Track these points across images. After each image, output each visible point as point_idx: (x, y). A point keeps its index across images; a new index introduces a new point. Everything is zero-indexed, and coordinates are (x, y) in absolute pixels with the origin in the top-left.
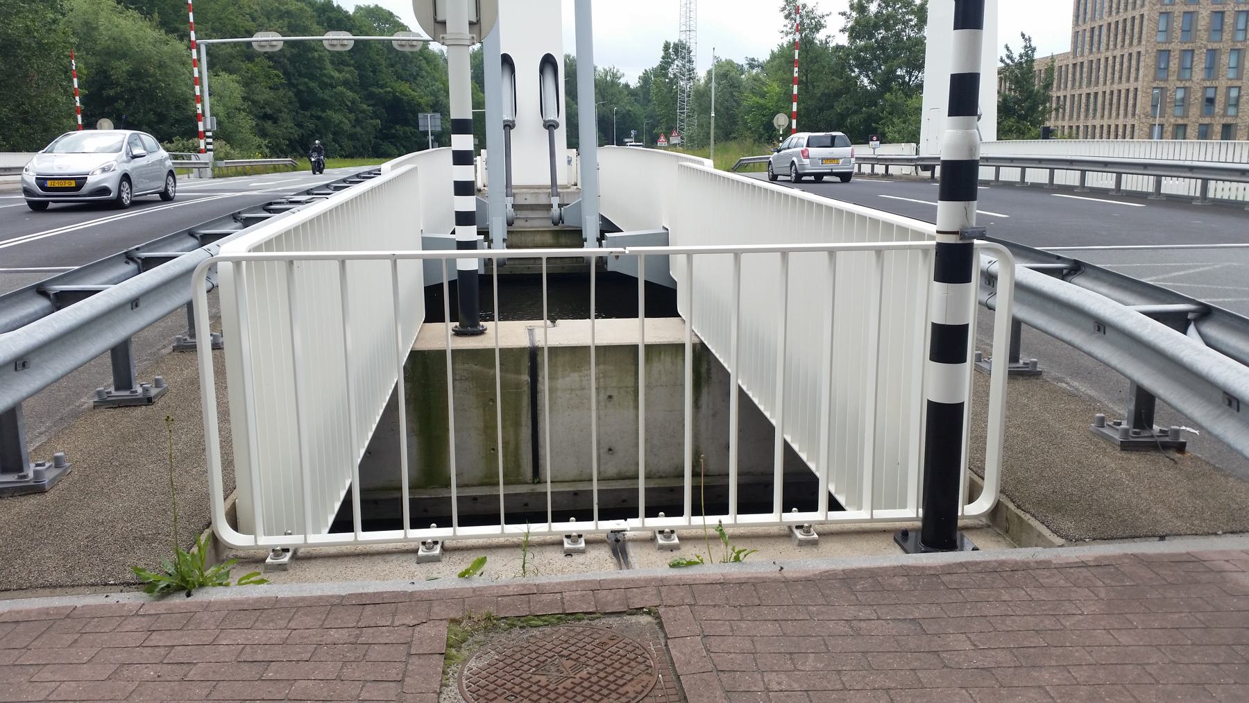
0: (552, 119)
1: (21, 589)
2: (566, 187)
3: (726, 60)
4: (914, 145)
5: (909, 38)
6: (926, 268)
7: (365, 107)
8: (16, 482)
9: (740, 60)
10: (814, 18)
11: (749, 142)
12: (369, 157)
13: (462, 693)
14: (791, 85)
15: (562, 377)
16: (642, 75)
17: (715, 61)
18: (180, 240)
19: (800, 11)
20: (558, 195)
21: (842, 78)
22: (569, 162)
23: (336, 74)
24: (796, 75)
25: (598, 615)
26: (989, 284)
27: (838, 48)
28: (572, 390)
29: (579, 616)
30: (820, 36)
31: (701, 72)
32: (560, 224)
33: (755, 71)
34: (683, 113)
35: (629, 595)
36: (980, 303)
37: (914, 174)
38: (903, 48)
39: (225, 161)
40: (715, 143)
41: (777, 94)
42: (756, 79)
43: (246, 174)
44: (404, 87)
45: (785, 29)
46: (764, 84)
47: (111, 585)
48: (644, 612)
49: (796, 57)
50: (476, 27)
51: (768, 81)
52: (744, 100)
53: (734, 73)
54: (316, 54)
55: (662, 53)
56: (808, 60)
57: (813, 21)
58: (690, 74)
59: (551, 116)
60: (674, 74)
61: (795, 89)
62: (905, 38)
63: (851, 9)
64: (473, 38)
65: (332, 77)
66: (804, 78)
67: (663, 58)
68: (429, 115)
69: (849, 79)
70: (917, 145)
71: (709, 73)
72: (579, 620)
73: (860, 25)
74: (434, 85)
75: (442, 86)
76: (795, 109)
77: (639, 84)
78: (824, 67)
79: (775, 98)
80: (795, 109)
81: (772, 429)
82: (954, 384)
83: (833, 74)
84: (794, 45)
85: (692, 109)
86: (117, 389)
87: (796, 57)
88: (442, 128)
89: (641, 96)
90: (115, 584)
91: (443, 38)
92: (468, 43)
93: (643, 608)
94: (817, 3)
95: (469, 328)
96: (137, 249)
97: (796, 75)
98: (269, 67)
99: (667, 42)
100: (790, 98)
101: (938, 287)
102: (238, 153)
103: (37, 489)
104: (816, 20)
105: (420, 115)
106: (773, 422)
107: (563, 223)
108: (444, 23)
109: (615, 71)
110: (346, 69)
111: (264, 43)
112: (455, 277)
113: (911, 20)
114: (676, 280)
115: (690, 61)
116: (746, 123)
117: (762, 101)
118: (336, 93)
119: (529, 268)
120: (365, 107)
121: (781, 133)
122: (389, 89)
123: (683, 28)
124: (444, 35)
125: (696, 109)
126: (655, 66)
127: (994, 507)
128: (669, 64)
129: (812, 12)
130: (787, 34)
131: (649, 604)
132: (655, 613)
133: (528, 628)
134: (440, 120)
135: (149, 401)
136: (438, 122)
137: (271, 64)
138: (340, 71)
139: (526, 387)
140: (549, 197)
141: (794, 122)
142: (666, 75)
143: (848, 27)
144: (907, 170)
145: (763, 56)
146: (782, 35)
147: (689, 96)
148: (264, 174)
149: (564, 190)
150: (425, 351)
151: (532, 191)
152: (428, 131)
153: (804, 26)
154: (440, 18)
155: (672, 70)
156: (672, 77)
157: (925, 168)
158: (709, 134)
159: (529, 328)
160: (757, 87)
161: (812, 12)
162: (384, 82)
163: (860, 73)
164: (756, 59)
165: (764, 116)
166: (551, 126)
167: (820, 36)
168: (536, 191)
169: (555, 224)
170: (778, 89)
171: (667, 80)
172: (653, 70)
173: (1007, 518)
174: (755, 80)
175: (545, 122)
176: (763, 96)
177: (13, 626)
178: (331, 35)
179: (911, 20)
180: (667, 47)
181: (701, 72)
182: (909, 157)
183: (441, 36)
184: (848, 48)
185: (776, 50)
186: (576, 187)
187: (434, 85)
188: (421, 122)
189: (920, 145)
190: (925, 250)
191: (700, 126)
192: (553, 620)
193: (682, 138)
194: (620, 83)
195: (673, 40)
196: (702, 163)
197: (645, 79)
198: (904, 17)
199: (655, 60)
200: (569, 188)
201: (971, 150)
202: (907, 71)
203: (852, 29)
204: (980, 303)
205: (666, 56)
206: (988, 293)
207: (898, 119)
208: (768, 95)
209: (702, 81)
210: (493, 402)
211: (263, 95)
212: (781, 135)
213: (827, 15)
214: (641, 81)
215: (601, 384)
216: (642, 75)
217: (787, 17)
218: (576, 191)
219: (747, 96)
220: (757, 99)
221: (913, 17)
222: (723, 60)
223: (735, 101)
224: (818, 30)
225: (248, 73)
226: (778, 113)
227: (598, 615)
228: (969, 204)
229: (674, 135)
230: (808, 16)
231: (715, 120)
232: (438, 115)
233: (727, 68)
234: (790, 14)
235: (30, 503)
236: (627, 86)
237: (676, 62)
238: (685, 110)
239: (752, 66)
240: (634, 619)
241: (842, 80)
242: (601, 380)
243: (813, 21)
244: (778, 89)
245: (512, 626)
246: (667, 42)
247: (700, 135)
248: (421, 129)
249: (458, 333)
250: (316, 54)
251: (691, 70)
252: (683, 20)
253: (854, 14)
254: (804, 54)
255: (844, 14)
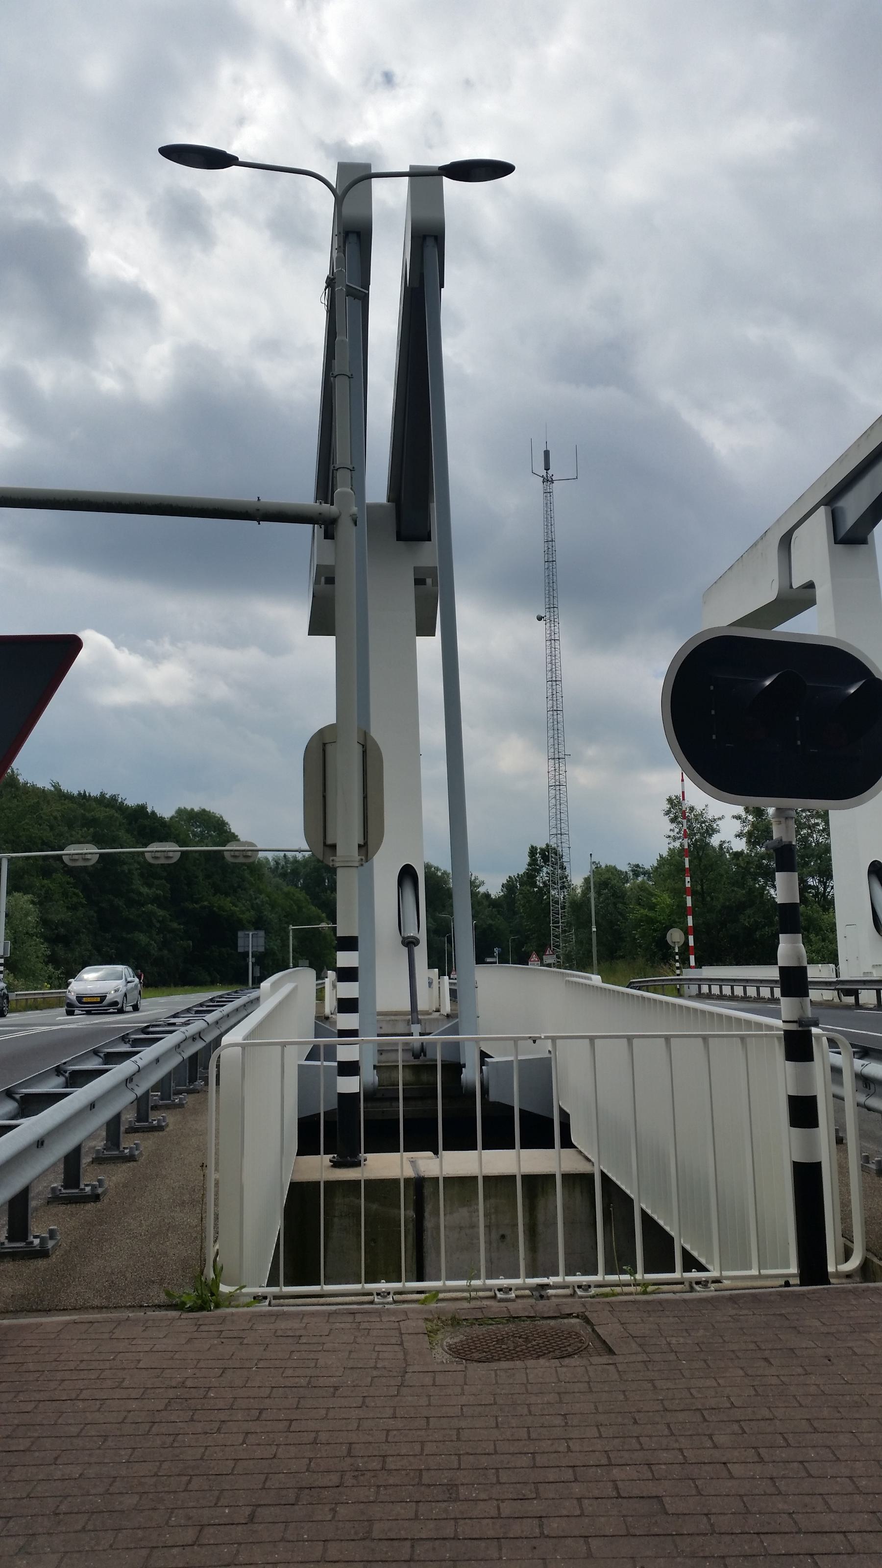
0: (412, 934)
1: (75, 1309)
2: (427, 1013)
3: (606, 866)
4: (832, 966)
5: (818, 843)
6: (779, 1051)
7: (175, 925)
8: (25, 1247)
9: (623, 867)
10: (704, 822)
11: (640, 961)
12: (176, 985)
13: (444, 1350)
14: (684, 896)
15: (450, 1213)
16: (505, 882)
17: (594, 867)
18: (88, 1058)
19: (687, 814)
20: (419, 1022)
21: (744, 889)
22: (430, 984)
23: (145, 890)
24: (688, 885)
25: (537, 1318)
26: (866, 1087)
27: (738, 855)
28: (461, 1228)
29: (523, 1318)
30: (715, 841)
31: (577, 880)
32: (422, 1058)
33: (640, 879)
34: (558, 927)
35: (560, 1308)
36: (858, 1105)
37: (837, 1000)
38: (812, 855)
39: (16, 993)
40: (599, 963)
41: (668, 906)
42: (642, 887)
43: (37, 1008)
44: (226, 903)
45: (672, 834)
46: (652, 895)
47: (146, 1306)
48: (573, 1317)
49: (687, 866)
50: (363, 850)
51: (657, 892)
52: (630, 913)
53: (615, 881)
54: (126, 868)
55: (528, 860)
56: (703, 868)
57: (703, 825)
58: (565, 885)
59: (411, 932)
60: (544, 883)
61: (689, 901)
62: (814, 844)
63: (747, 812)
64: (362, 860)
65: (140, 894)
66: (699, 888)
67: (529, 865)
68: (251, 934)
69: (751, 890)
70: (836, 966)
71: (587, 880)
72: (524, 1321)
73: (758, 830)
74: (259, 898)
75: (267, 899)
76: (690, 923)
77: (502, 894)
78: (722, 876)
79: (667, 911)
80: (690, 923)
81: (671, 1239)
82: (811, 1145)
83: (733, 885)
84: (682, 852)
85: (568, 922)
86: (65, 1187)
87: (687, 866)
88: (265, 949)
89: (505, 906)
90: (148, 1306)
91: (333, 860)
92: (357, 864)
93: (572, 1314)
94: (706, 806)
95: (348, 1159)
96: (65, 1063)
97: (688, 885)
98: (68, 883)
99: (532, 847)
100: (683, 911)
101: (789, 1064)
102: (22, 985)
103: (43, 1253)
104: (707, 824)
105: (240, 934)
106: (672, 1234)
107: (425, 1055)
108: (333, 847)
109: (473, 878)
110: (157, 882)
111: (76, 857)
112: (334, 1104)
113: (818, 824)
114: (568, 1111)
115: (563, 868)
116: (635, 939)
117: (651, 914)
118: (144, 912)
119: (383, 1112)
120: (175, 925)
121: (677, 951)
122: (206, 903)
123: (554, 831)
124: (334, 858)
125: (573, 922)
126: (521, 873)
127: (862, 1263)
128: (539, 871)
129: (702, 814)
130: (675, 839)
131: (576, 1312)
132: (582, 1316)
133: (486, 1326)
134: (263, 939)
135: (96, 1198)
136: (262, 941)
137: (72, 880)
138: (150, 886)
139: (411, 1224)
140: (408, 1025)
141: (691, 938)
142: (534, 885)
143: (744, 831)
144: (828, 995)
145: (649, 862)
146: (668, 840)
147: (563, 908)
148: (57, 1007)
149: (426, 1017)
150: (303, 1182)
151: (388, 1018)
152: (248, 953)
153: (693, 831)
154: (329, 841)
155: (543, 876)
156: (541, 885)
157: (848, 993)
158: (591, 951)
159: (412, 1160)
160: (643, 897)
161: (702, 814)
162: (201, 896)
163: (766, 883)
164: (641, 866)
165: (655, 930)
166: (410, 943)
167: (715, 841)
168: (393, 1018)
169: (416, 1056)
170: (669, 901)
171: (535, 889)
172: (518, 877)
173: (873, 1271)
174: (642, 890)
175: (404, 938)
176: (652, 907)
177: (87, 1325)
178: (154, 847)
179: (818, 824)
180: (533, 851)
181: (577, 880)
182: (827, 980)
183: (331, 858)
184: (748, 855)
185: (665, 854)
186: (438, 1013)
187: (259, 898)
188: (240, 942)
189: (840, 965)
190: (779, 1038)
191: (579, 942)
192: (505, 1321)
193: (558, 957)
194: (479, 892)
195: (541, 845)
196: (590, 979)
197: (509, 887)
198: (809, 820)
199: (520, 865)
200: (430, 1014)
201: (799, 959)
202: (820, 881)
203: (750, 835)
204: (858, 1105)
205: (533, 862)
206: (865, 1096)
207: (817, 935)
208: (658, 907)
209: (579, 891)
210: (375, 1243)
211: (59, 913)
212: (677, 954)
213: (719, 819)
214: (505, 889)
215: (493, 1220)
216: (505, 882)
217: (673, 821)
218: (440, 1017)
219: (633, 909)
220: (645, 912)
221: (819, 821)
222: (603, 866)
223: (621, 914)
224: (710, 835)
225: (41, 890)
226: (672, 927)
227: (537, 1318)
228: (803, 1000)
229: (547, 953)
230: (697, 819)
231: (597, 936)
232: (262, 933)
233: (606, 876)
234: (676, 818)
235: (41, 1263)
236: (487, 896)
237: (545, 869)
238: (560, 924)
239: (636, 873)
240: (566, 1321)
241: (744, 892)
242: (493, 1217)
243: (703, 825)
244: (669, 901)
245: (472, 1324)
246: (532, 847)
247: (579, 953)
248: (240, 950)
249: (336, 1165)
250: (126, 868)
251: (564, 877)
252: (553, 822)
253: (750, 818)
254: (696, 862)
255: (738, 817)
